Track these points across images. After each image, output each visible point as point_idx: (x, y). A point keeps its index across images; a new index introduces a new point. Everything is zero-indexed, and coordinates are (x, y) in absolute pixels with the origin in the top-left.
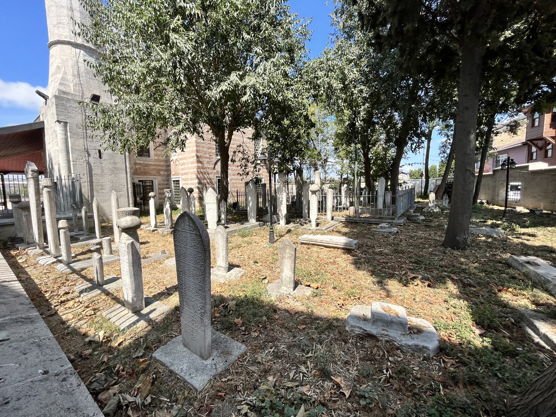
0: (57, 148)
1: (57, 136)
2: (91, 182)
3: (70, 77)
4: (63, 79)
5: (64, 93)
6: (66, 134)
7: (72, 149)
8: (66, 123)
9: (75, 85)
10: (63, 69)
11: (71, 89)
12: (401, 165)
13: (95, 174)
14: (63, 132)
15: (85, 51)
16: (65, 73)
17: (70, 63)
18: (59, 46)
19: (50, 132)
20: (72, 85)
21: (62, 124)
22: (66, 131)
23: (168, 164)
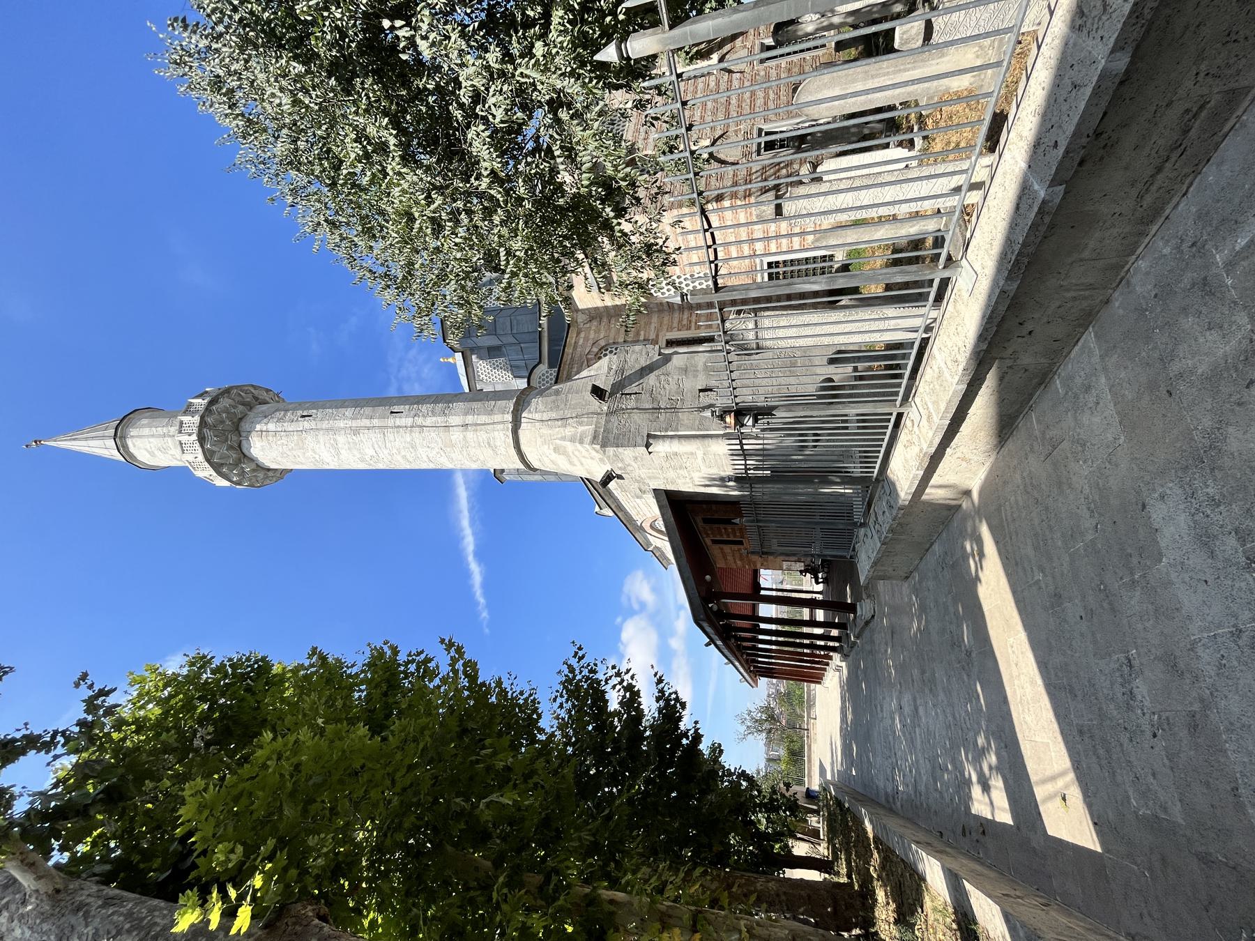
0: (700, 454)
1: (676, 454)
2: (851, 209)
3: (569, 431)
4: (572, 440)
5: (595, 438)
6: (672, 437)
7: (699, 429)
8: (649, 436)
9: (581, 424)
10: (558, 442)
11: (590, 429)
12: (990, 817)
13: (1037, 783)
14: (668, 442)
15: (522, 411)
16: (563, 439)
17: (545, 431)
18: (523, 448)
19: (671, 474)
20: (581, 429)
21: (651, 441)
22: (664, 437)
23: (666, 307)
